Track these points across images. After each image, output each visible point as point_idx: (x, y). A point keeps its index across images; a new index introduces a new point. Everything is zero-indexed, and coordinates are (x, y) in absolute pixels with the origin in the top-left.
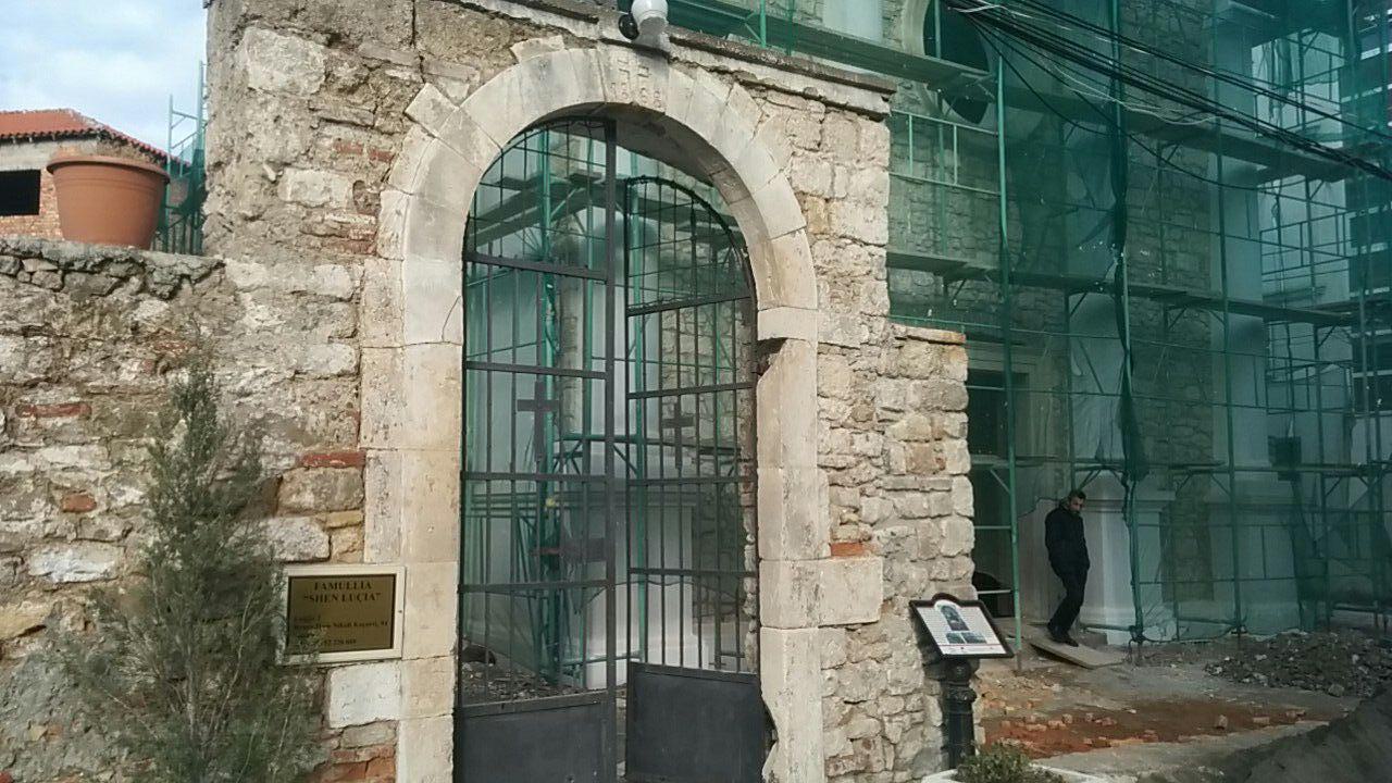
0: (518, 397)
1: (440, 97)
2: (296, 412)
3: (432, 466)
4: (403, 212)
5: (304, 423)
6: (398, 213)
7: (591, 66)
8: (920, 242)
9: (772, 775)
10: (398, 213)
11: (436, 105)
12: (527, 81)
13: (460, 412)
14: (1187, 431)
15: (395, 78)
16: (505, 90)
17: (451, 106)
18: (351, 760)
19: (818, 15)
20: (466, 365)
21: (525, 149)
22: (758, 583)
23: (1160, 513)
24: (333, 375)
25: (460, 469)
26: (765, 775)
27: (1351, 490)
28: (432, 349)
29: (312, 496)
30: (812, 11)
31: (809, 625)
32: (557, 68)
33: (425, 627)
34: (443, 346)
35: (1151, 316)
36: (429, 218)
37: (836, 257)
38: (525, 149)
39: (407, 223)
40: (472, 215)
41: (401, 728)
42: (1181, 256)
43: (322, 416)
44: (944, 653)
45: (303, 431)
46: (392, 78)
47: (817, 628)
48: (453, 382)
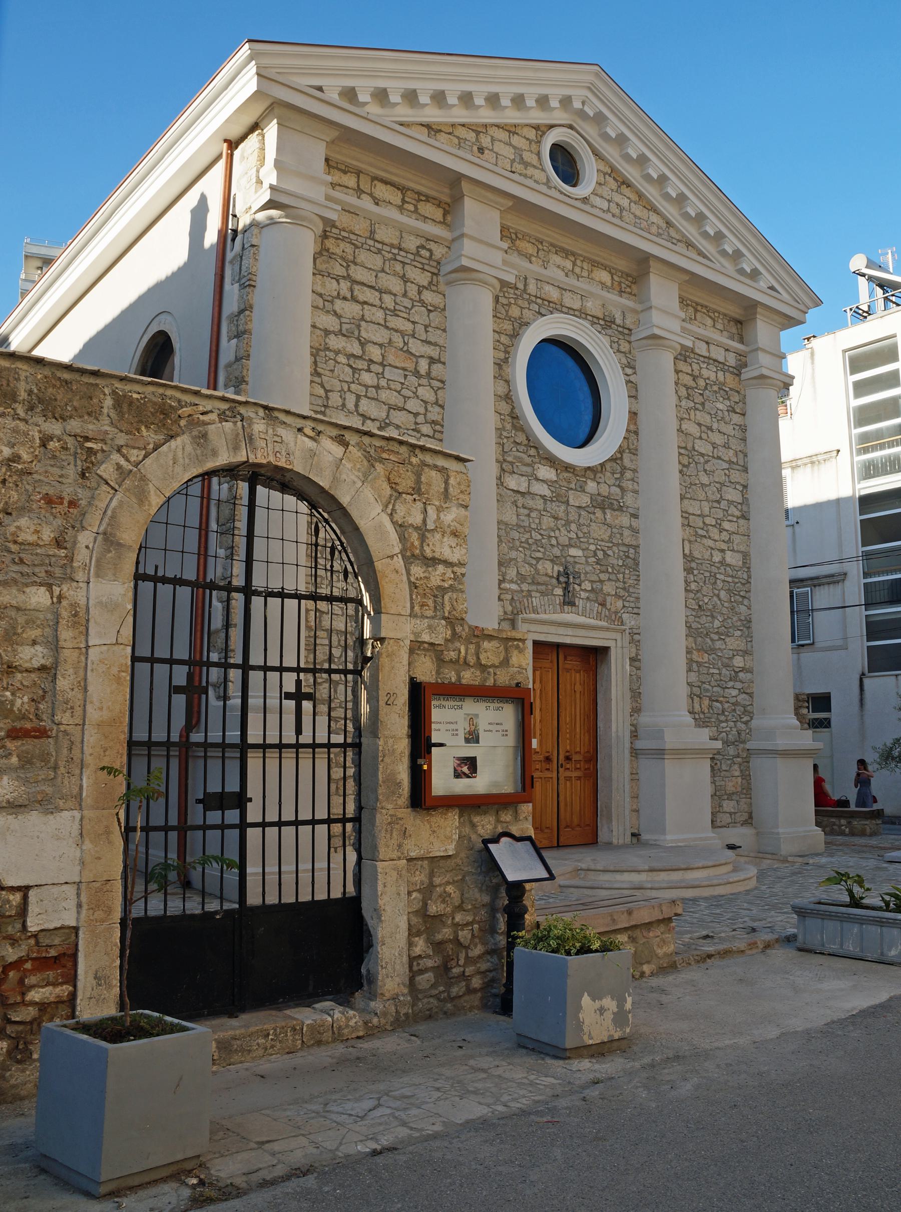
0: (174, 684)
1: (123, 462)
2: (7, 696)
3: (106, 737)
4: (91, 547)
5: (13, 705)
6: (87, 547)
7: (238, 435)
8: (523, 540)
9: (368, 971)
10: (87, 547)
11: (119, 467)
12: (189, 448)
13: (128, 697)
14: (734, 692)
15: (91, 448)
16: (171, 456)
17: (131, 467)
18: (44, 955)
19: (442, 360)
20: (135, 659)
21: (186, 495)
22: (360, 825)
23: (711, 758)
24: (34, 669)
25: (127, 739)
26: (363, 971)
27: (599, 833)
28: (108, 650)
29: (17, 759)
30: (437, 357)
31: (399, 858)
32: (211, 436)
33: (99, 858)
34: (116, 648)
35: (706, 601)
36: (110, 551)
37: (427, 575)
38: (186, 495)
39: (94, 555)
40: (144, 545)
41: (81, 934)
42: (729, 553)
43: (26, 699)
44: (510, 880)
45: (11, 711)
46: (88, 448)
47: (405, 861)
48: (124, 674)
